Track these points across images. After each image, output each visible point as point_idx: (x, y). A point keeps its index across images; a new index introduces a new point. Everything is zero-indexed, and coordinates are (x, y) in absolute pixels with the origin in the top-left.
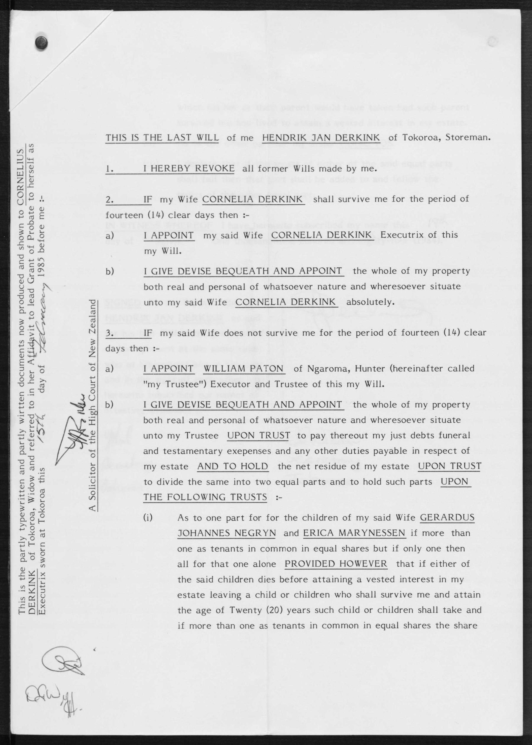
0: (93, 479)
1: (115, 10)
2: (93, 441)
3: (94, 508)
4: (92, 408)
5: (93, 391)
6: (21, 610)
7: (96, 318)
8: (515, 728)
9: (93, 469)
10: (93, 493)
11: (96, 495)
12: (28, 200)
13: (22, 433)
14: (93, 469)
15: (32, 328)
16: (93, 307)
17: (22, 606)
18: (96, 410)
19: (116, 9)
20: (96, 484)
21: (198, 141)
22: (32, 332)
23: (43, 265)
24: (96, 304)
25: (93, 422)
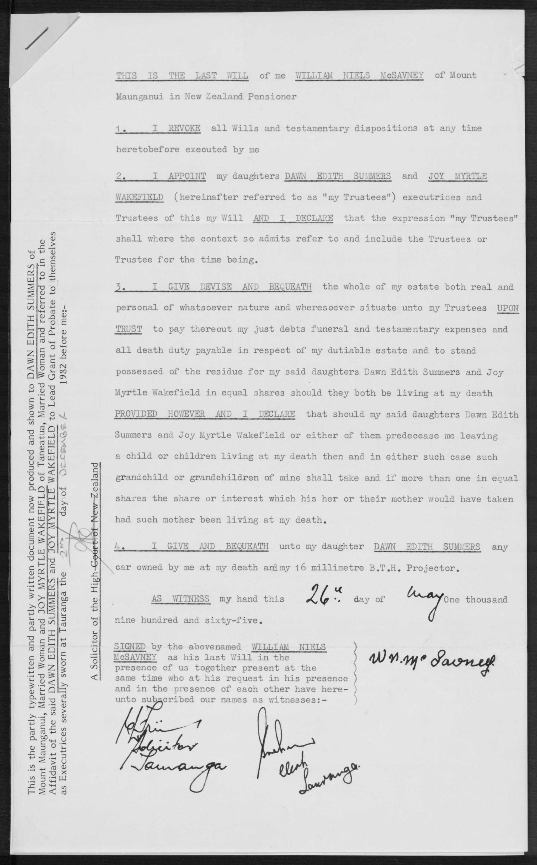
0: (95, 648)
2: (95, 609)
3: (96, 677)
4: (95, 575)
6: (31, 790)
7: (99, 481)
8: (517, 844)
9: (95, 637)
10: (95, 661)
11: (98, 664)
12: (39, 280)
13: (32, 719)
14: (95, 637)
16: (95, 470)
17: (32, 786)
18: (99, 577)
20: (98, 652)
21: (56, 482)
23: (65, 372)
24: (98, 467)
25: (96, 590)
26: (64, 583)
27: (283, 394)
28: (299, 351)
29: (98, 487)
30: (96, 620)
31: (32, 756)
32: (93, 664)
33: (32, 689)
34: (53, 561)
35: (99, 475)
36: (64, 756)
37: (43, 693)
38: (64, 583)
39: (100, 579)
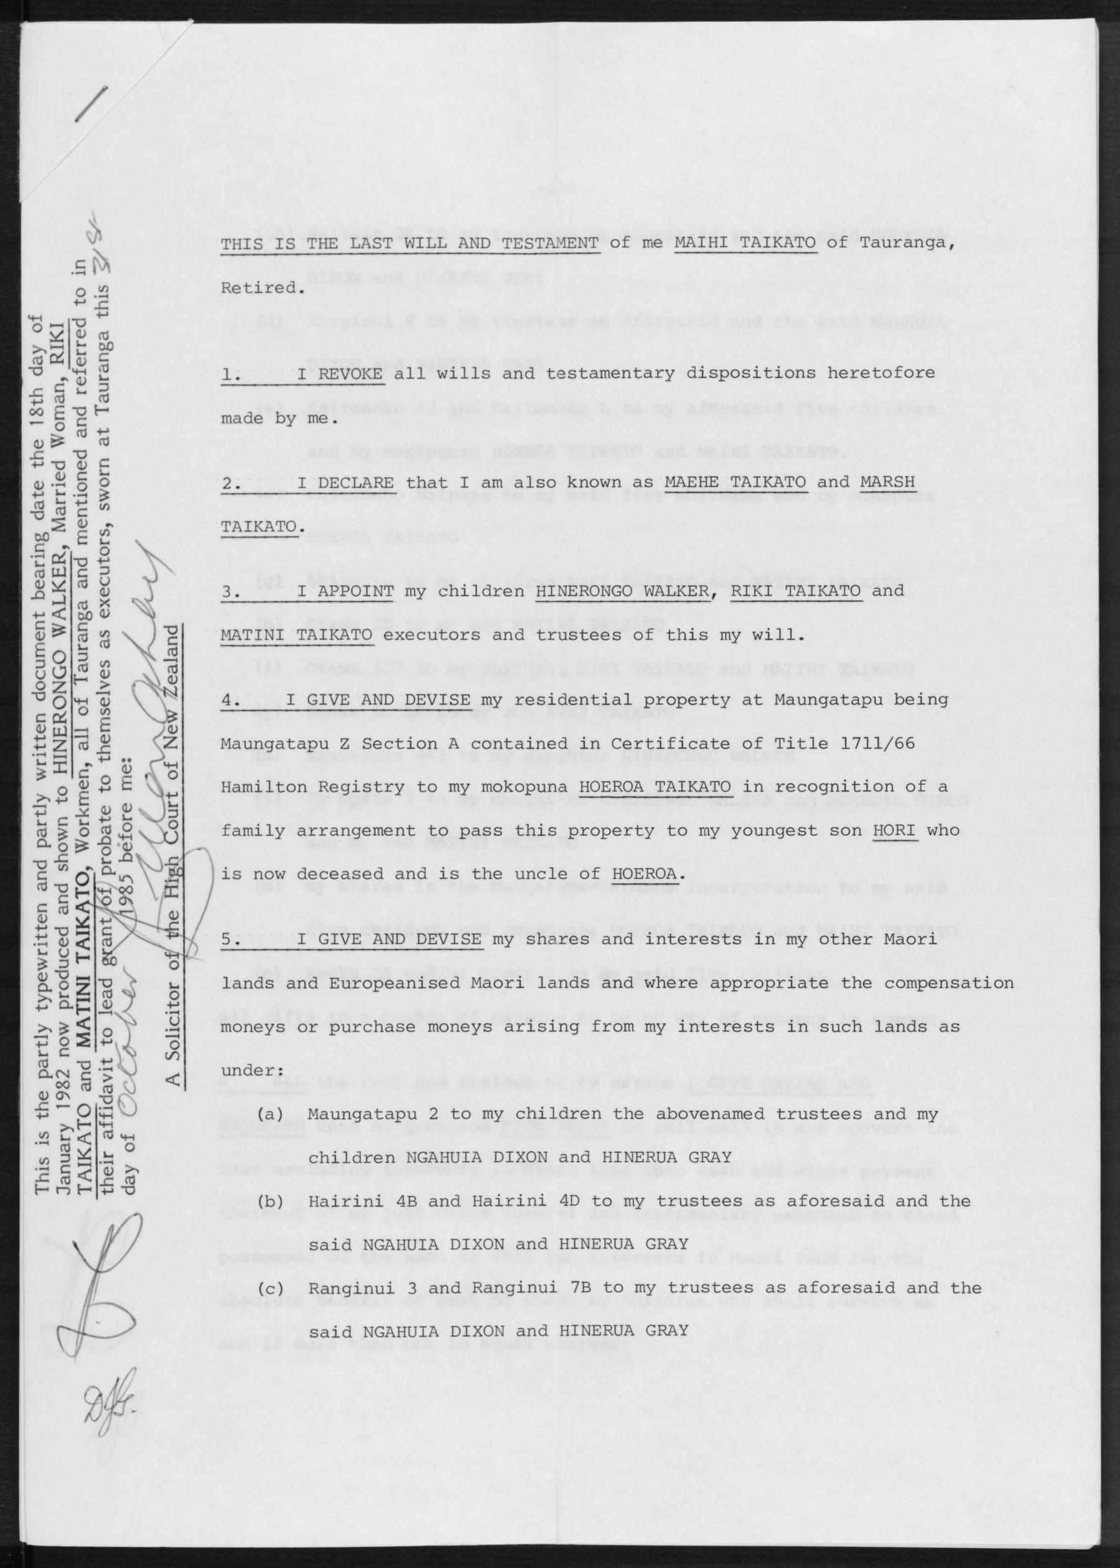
0: (175, 1016)
1: (198, 20)
3: (177, 1080)
5: (173, 825)
6: (41, 1185)
7: (179, 664)
9: (174, 995)
10: (175, 1045)
11: (181, 1050)
13: (42, 803)
14: (174, 995)
15: (107, 1065)
16: (172, 641)
18: (181, 865)
19: (201, 17)
22: (108, 1073)
26: (108, 1189)
27: (585, 940)
28: (615, 243)
29: (179, 674)
30: (174, 768)
31: (43, 1113)
32: (170, 1051)
33: (43, 971)
34: (83, 562)
35: (180, 650)
36: (105, 570)
37: (61, 498)
38: (108, 1189)
39: (183, 869)
